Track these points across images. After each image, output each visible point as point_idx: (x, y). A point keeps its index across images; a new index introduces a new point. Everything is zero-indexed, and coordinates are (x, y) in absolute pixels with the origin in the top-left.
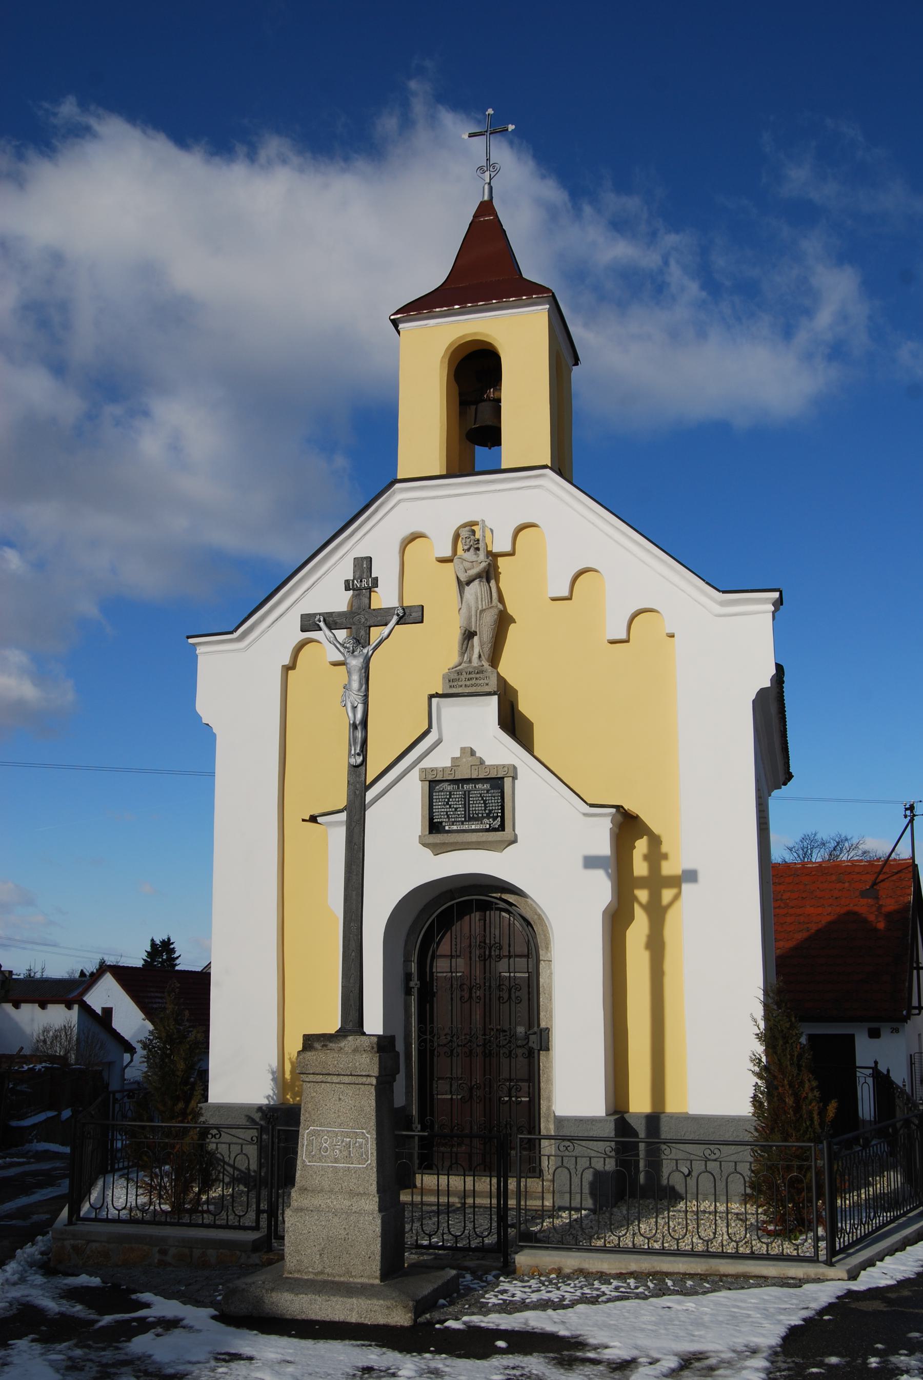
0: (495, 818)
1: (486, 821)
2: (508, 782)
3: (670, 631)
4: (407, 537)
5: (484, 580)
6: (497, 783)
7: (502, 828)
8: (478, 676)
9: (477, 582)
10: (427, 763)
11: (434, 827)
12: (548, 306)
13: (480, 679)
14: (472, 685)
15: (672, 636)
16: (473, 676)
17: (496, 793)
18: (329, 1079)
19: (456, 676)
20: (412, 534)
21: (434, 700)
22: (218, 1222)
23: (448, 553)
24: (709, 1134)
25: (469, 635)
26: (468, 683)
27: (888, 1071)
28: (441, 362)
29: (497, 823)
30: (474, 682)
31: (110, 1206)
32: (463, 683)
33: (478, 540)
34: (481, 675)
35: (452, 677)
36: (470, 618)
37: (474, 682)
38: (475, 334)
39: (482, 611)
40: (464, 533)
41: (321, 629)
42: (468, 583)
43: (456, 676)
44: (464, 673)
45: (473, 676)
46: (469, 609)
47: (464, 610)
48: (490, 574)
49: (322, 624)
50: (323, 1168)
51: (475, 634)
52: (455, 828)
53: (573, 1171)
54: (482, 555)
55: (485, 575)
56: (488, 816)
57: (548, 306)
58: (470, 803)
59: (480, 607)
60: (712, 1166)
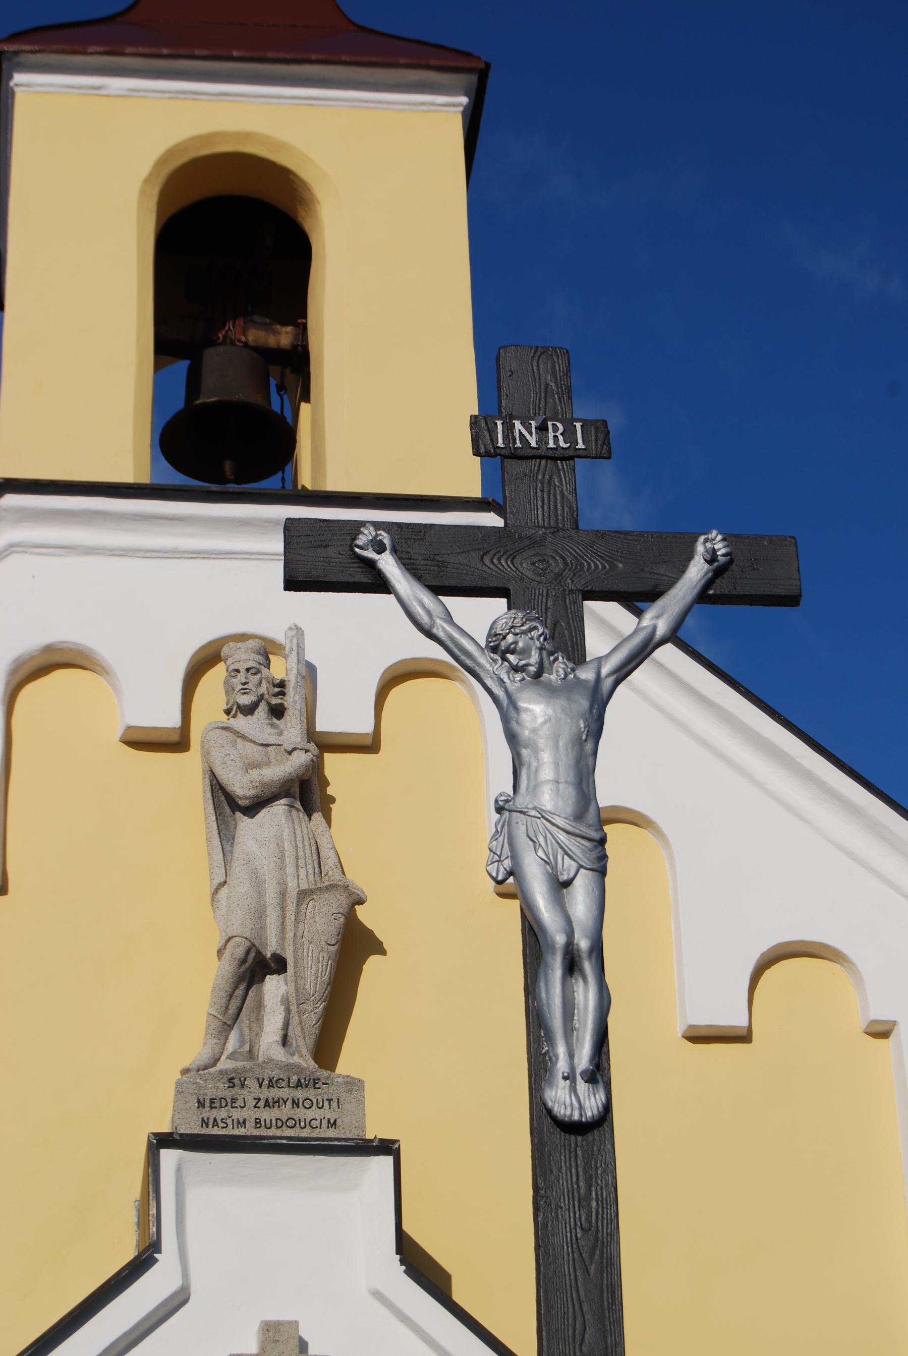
3: (880, 1012)
4: (31, 658)
5: (298, 804)
8: (300, 1094)
9: (279, 808)
12: (464, 100)
13: (309, 1104)
15: (881, 1032)
16: (284, 1093)
19: (222, 1090)
20: (49, 649)
21: (169, 1157)
23: (169, 718)
25: (257, 967)
28: (143, 192)
33: (282, 684)
34: (311, 1093)
35: (210, 1093)
36: (260, 914)
37: (286, 1111)
38: (247, 136)
39: (304, 895)
40: (243, 656)
41: (380, 585)
42: (252, 808)
43: (222, 1090)
44: (251, 1083)
45: (284, 1093)
46: (258, 884)
47: (240, 886)
48: (307, 793)
49: (388, 564)
51: (279, 965)
54: (292, 730)
55: (296, 790)
57: (464, 100)
59: (292, 885)
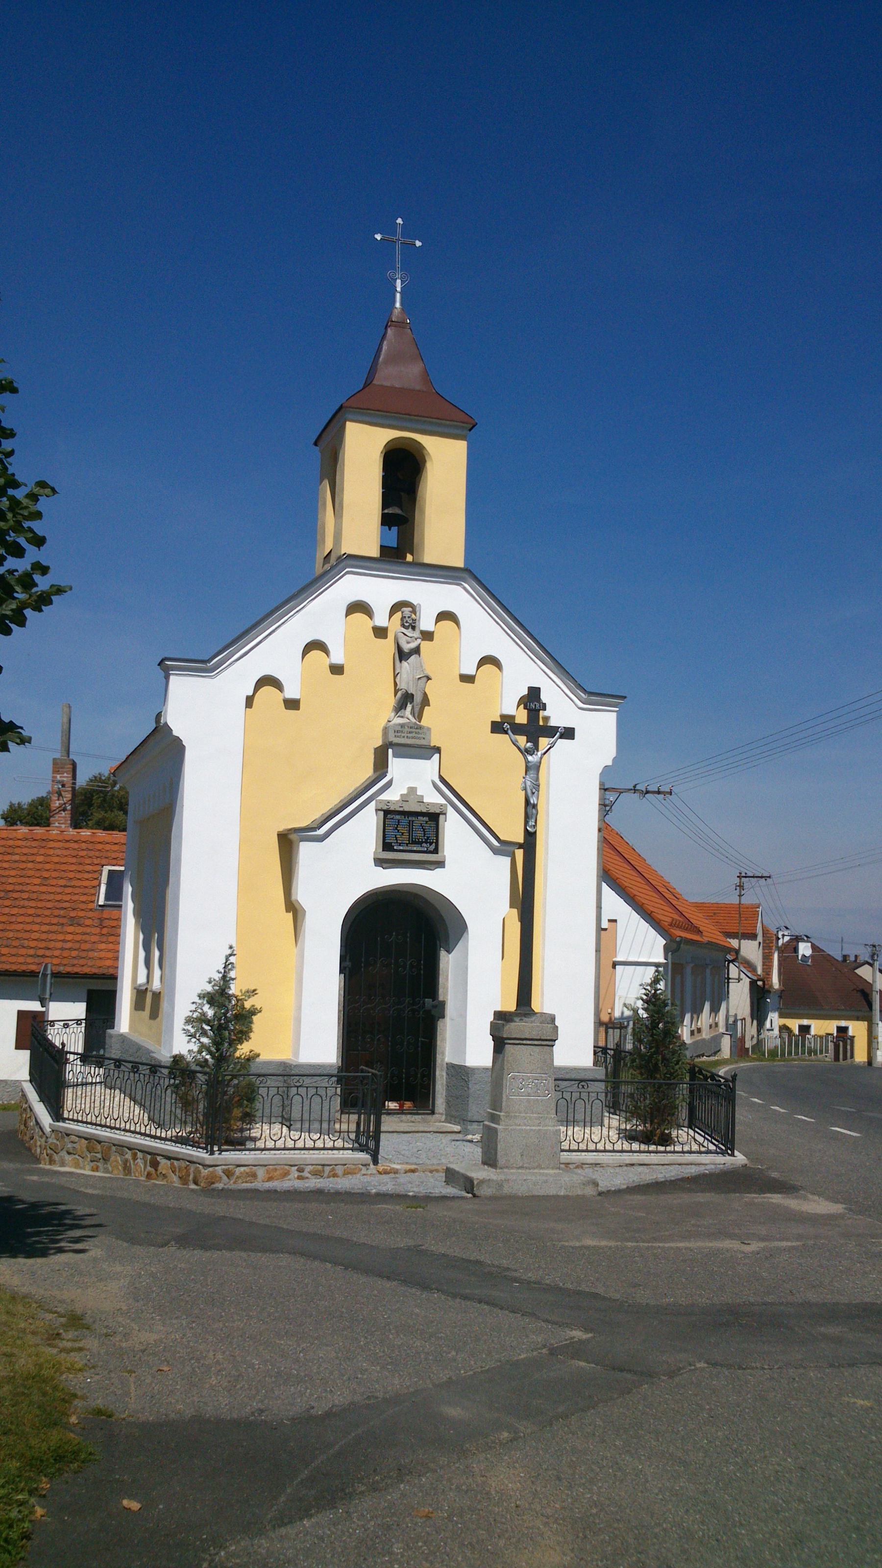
0: (431, 844)
1: (424, 845)
2: (441, 817)
6: (434, 817)
7: (436, 851)
10: (384, 797)
11: (387, 846)
14: (413, 738)
17: (433, 824)
18: (524, 1042)
22: (277, 1146)
24: (315, 1072)
26: (409, 735)
27: (63, 1044)
29: (432, 847)
30: (414, 735)
31: (268, 1138)
32: (406, 735)
37: (414, 735)
43: (399, 728)
50: (520, 1100)
52: (401, 848)
53: (305, 1097)
56: (426, 843)
58: (411, 832)
60: (302, 1091)
